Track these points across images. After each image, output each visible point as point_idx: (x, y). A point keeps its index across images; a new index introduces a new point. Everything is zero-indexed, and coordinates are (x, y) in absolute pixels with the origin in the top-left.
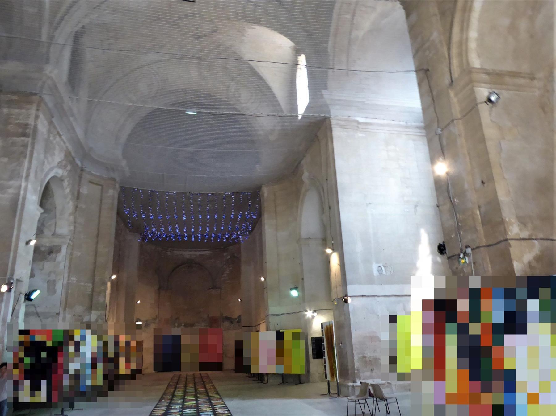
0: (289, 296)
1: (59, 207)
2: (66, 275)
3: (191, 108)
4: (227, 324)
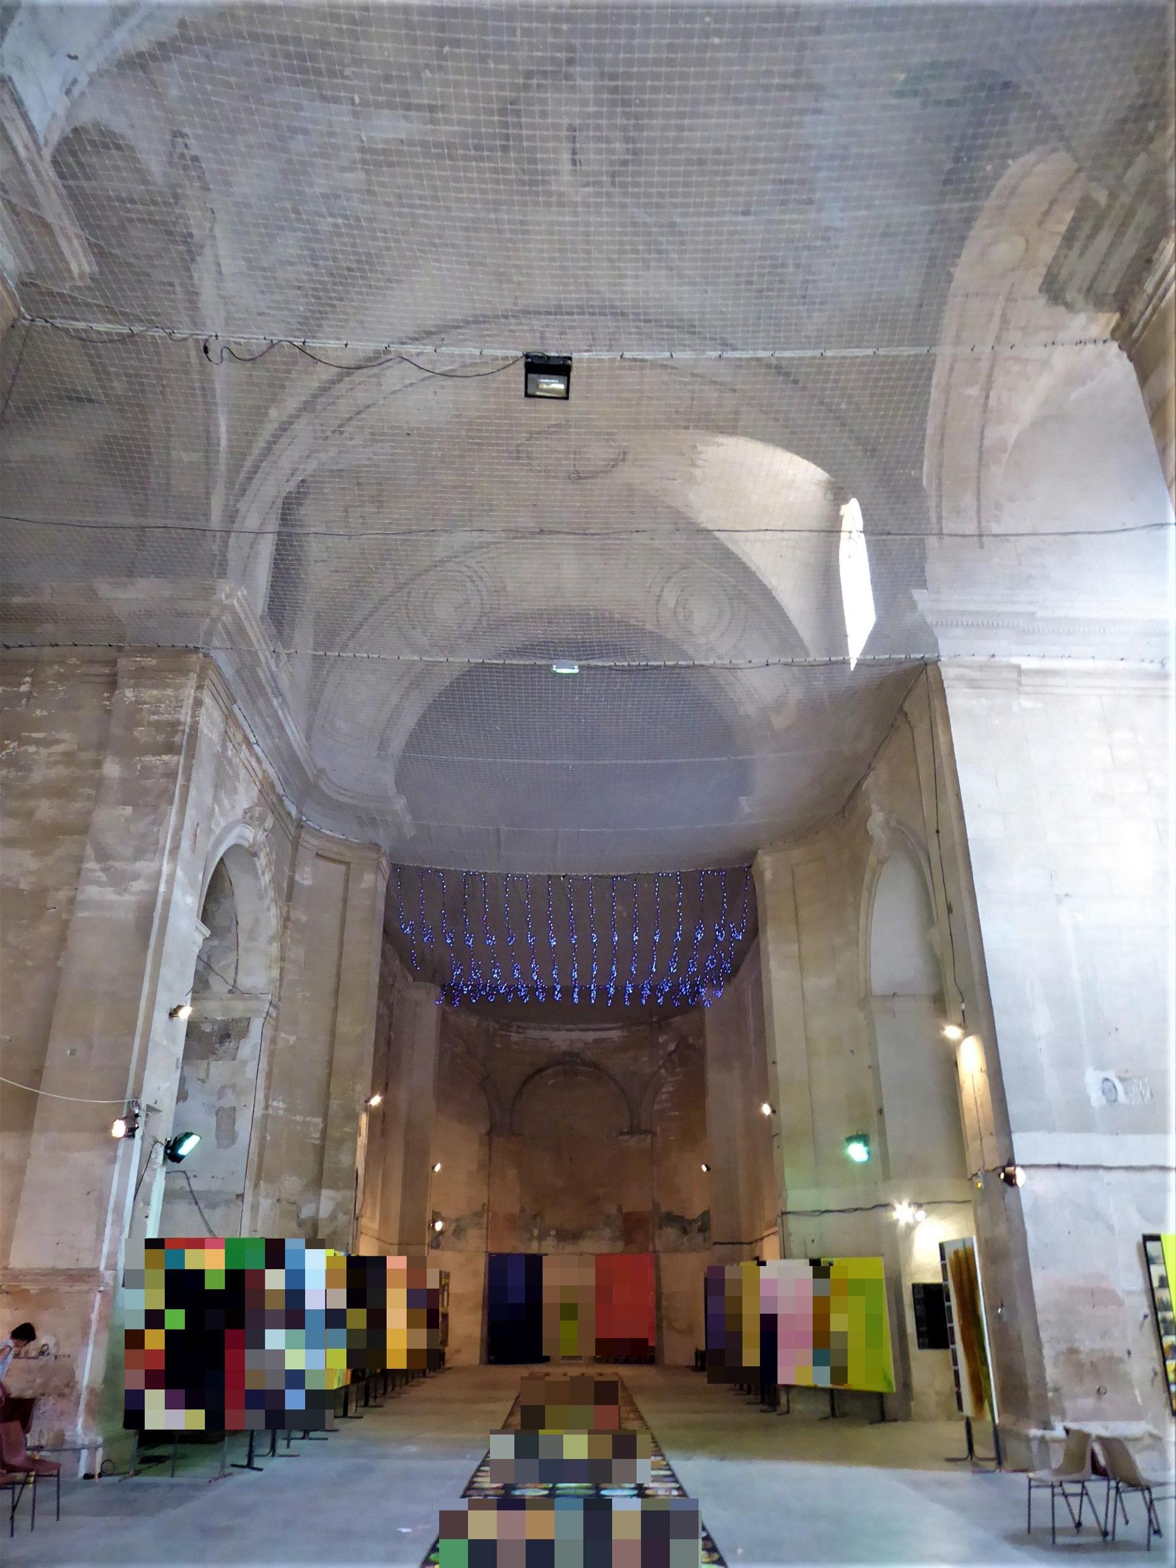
0: (846, 1161)
1: (245, 921)
2: (260, 1095)
3: (564, 657)
4: (671, 1233)
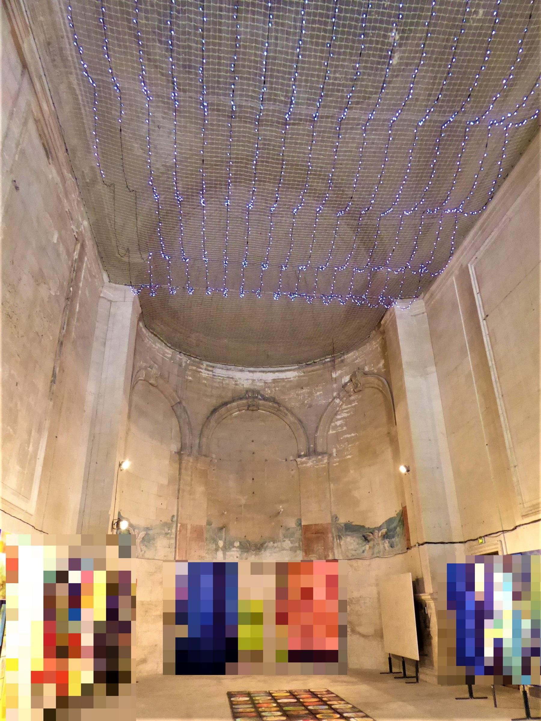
4: (351, 542)
